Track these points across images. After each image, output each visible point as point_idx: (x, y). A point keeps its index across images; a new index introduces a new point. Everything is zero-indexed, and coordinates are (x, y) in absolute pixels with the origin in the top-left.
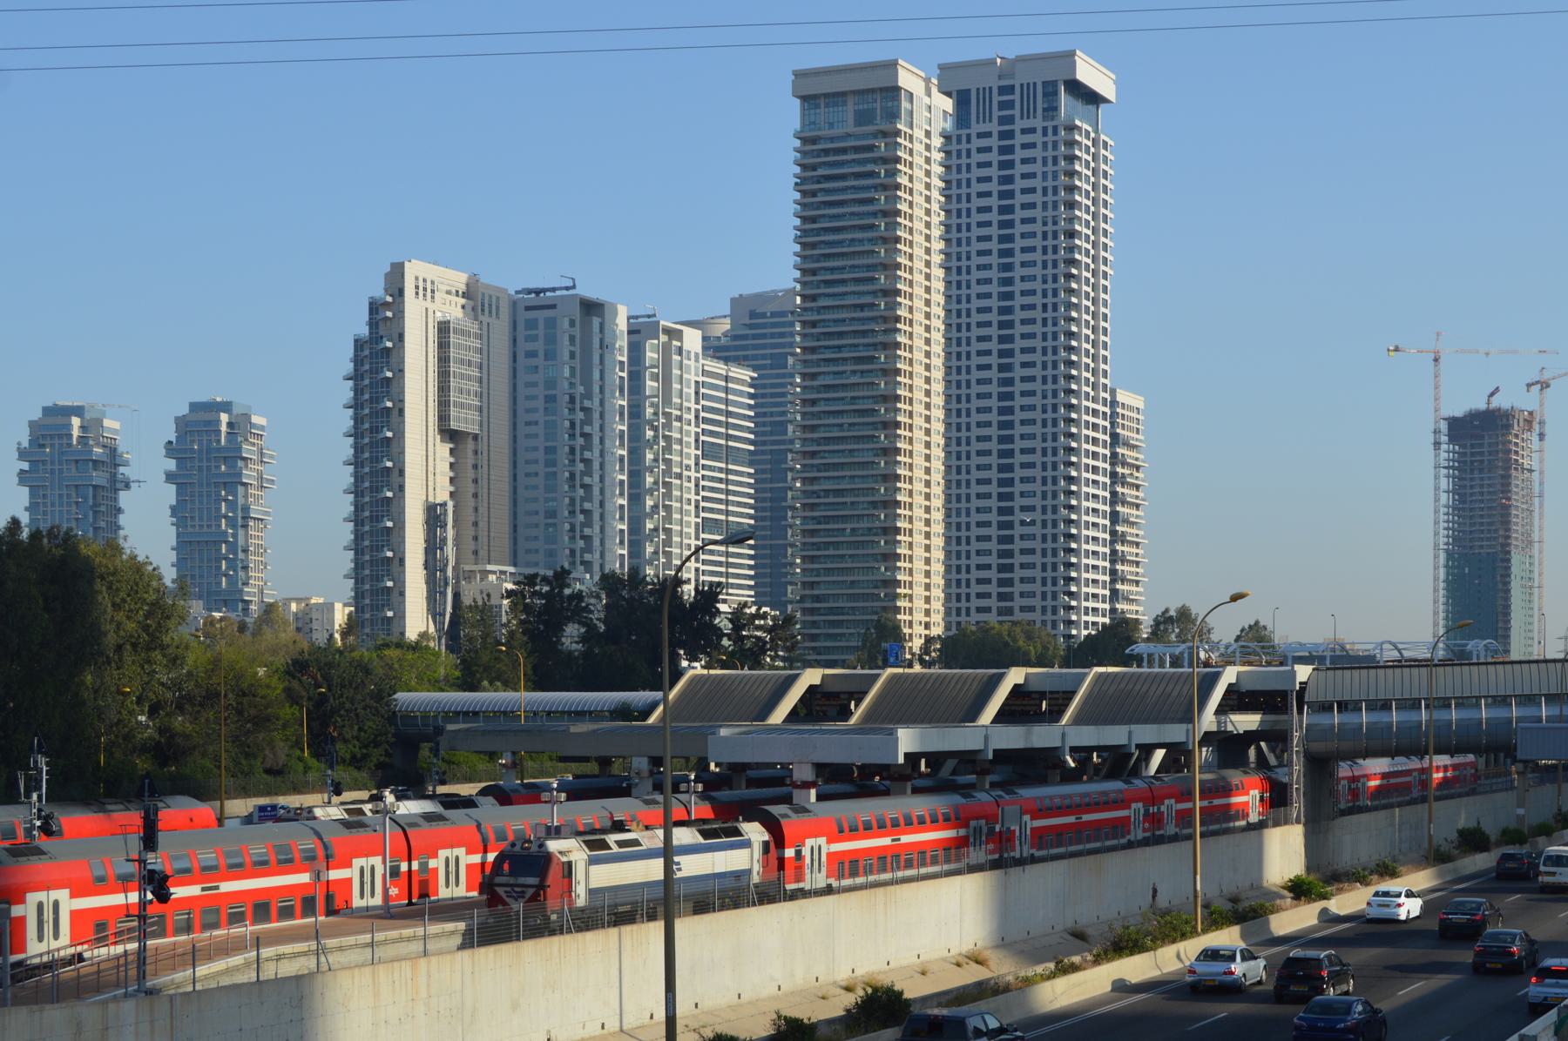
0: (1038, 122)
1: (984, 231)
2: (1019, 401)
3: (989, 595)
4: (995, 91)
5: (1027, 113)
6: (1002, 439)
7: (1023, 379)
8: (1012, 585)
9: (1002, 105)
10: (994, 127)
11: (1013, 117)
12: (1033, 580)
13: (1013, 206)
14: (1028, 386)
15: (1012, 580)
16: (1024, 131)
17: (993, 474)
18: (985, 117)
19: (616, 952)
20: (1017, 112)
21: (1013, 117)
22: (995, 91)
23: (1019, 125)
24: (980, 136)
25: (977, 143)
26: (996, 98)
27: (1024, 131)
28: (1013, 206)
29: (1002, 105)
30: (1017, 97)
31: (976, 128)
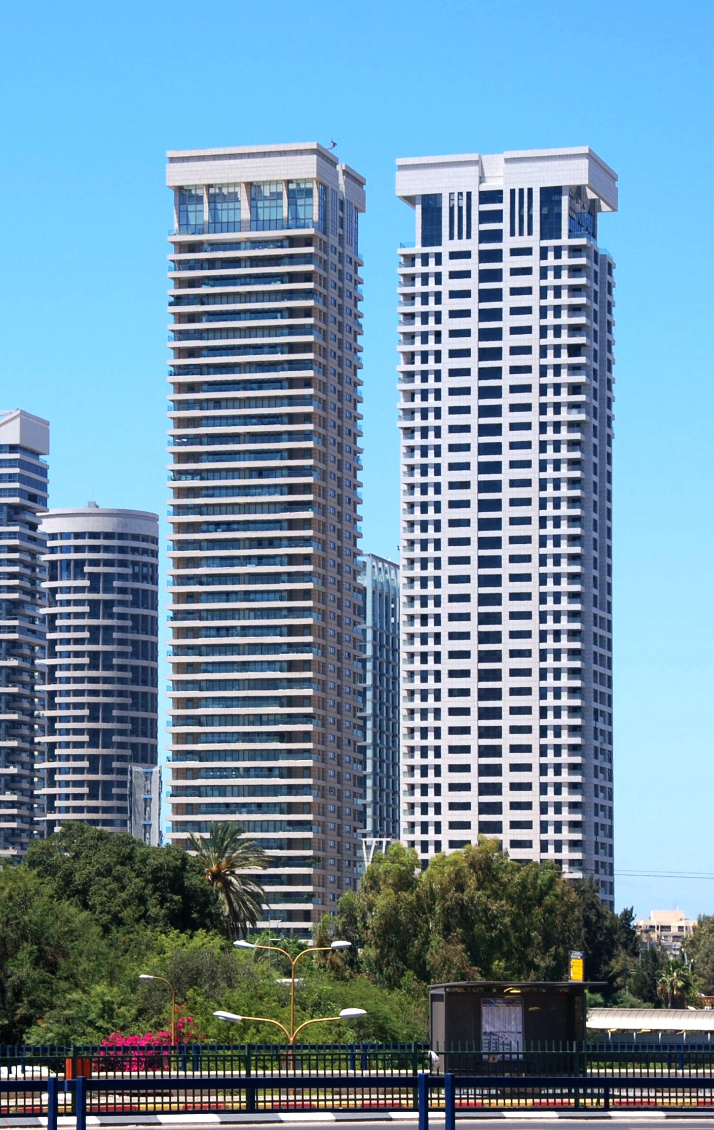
0: (534, 241)
1: (459, 495)
2: (508, 282)
3: (466, 523)
4: (475, 199)
5: (520, 227)
6: (485, 354)
7: (514, 673)
8: (500, 259)
9: (485, 217)
10: (473, 245)
11: (500, 232)
12: (527, 653)
13: (500, 271)
14: (520, 701)
15: (499, 634)
16: (515, 252)
17: (472, 284)
18: (461, 230)
19: (143, 522)
20: (505, 226)
21: (500, 232)
22: (475, 199)
23: (507, 243)
24: (454, 255)
25: (449, 265)
26: (477, 208)
27: (515, 252)
28: (500, 271)
29: (485, 217)
30: (505, 206)
31: (447, 246)
